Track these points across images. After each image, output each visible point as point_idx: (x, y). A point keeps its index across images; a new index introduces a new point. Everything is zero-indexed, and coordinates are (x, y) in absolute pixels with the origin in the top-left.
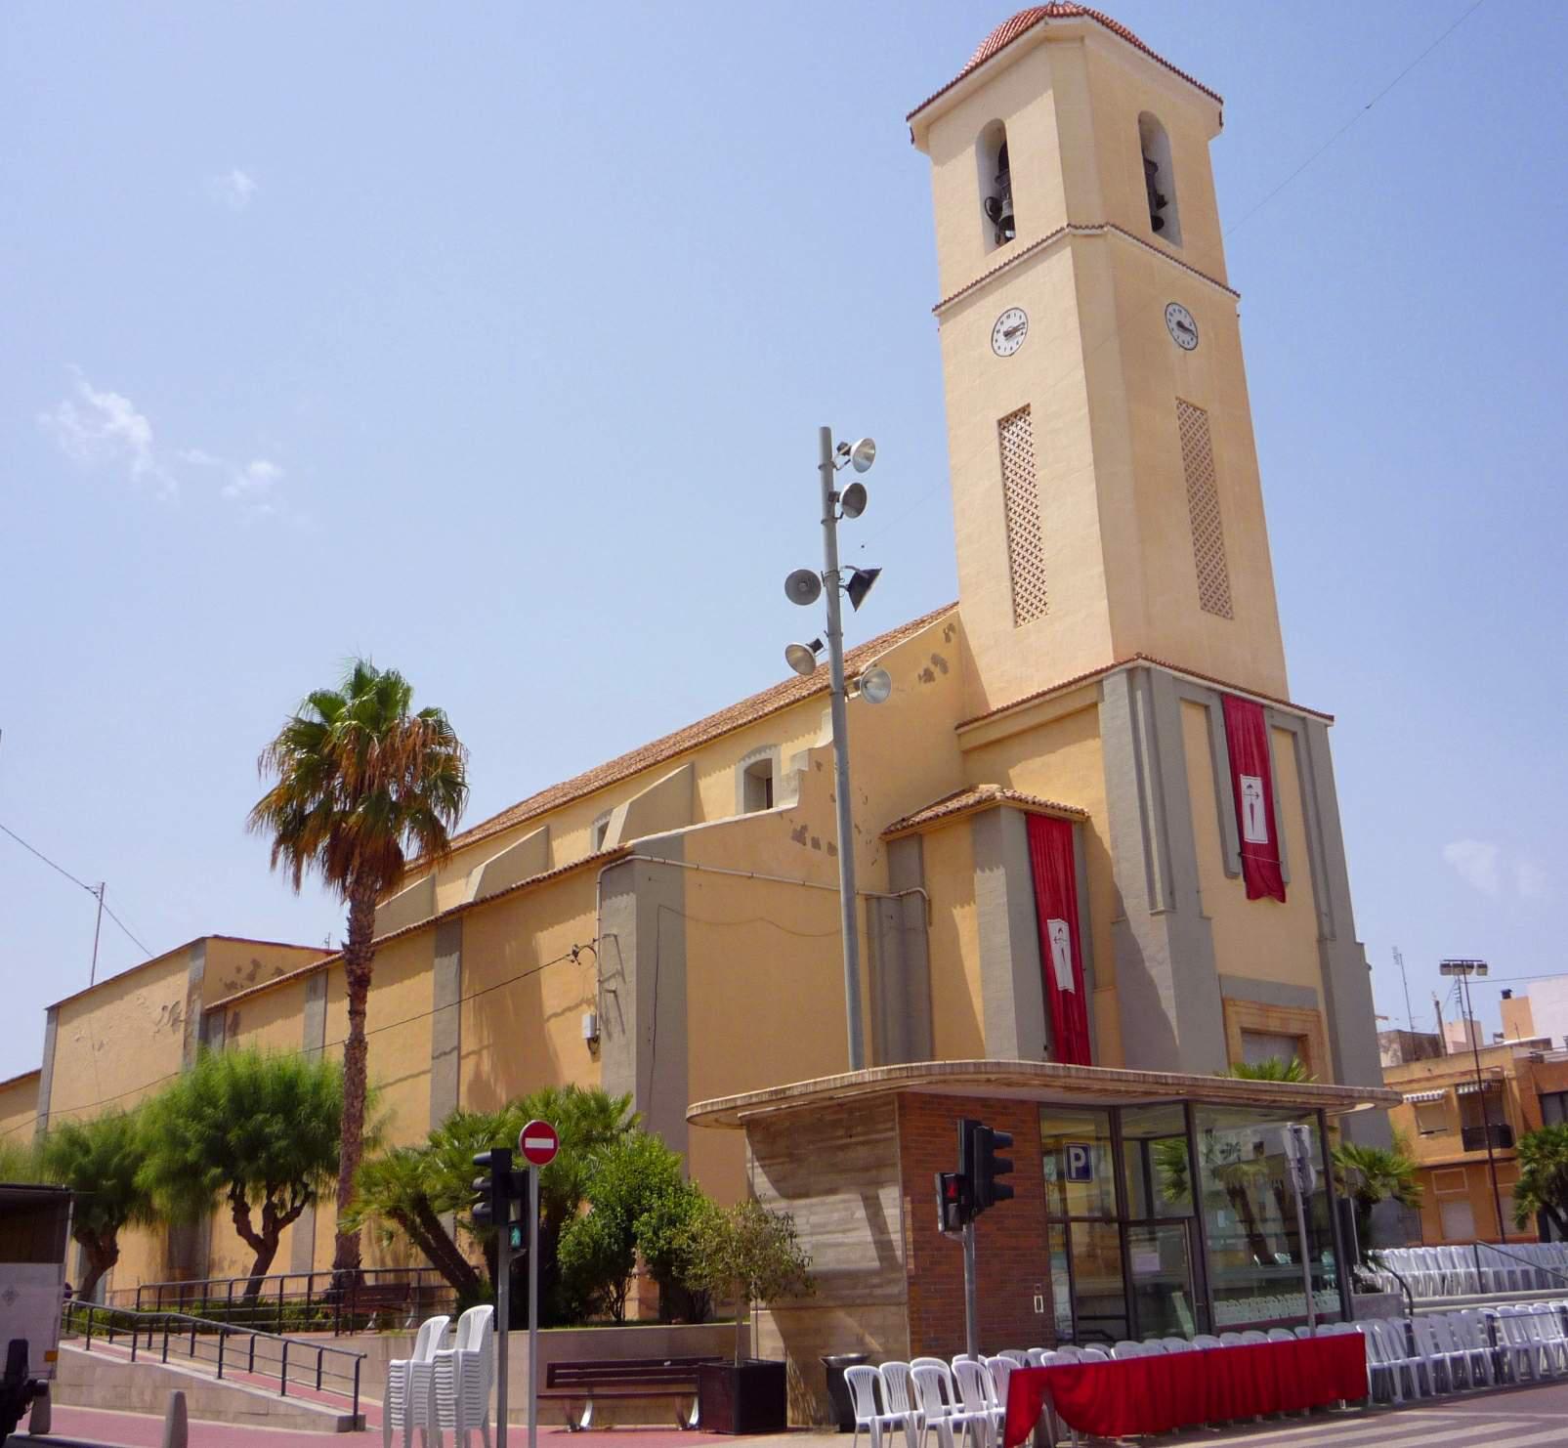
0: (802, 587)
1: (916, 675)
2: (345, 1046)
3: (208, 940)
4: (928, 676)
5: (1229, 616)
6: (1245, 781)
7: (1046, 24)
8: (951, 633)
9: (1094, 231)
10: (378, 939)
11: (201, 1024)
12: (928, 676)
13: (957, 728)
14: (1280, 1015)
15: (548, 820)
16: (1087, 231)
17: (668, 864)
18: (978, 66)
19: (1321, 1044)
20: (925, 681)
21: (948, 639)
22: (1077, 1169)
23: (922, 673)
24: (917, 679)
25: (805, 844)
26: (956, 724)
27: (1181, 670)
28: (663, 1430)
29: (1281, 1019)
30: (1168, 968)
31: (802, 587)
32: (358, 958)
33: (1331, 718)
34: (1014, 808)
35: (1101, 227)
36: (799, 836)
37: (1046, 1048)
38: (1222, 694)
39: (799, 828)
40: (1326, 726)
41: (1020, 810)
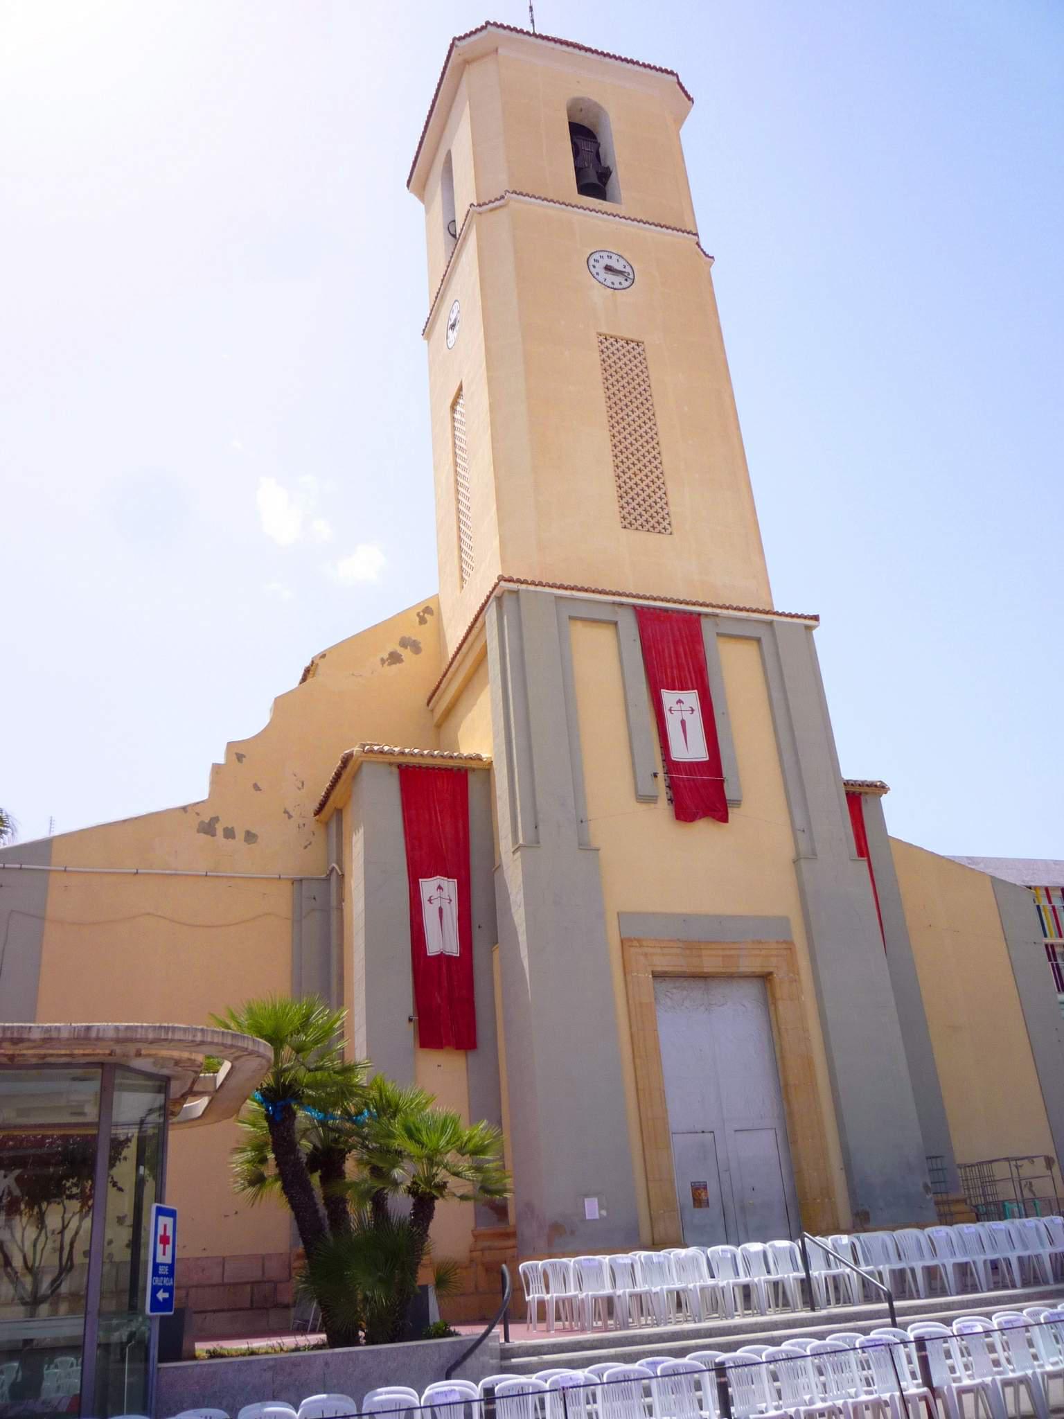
1: (378, 658)
4: (395, 658)
5: (668, 532)
9: (497, 203)
12: (395, 658)
14: (721, 953)
16: (491, 205)
17: (25, 869)
19: (795, 980)
20: (390, 664)
21: (422, 621)
23: (386, 656)
25: (213, 835)
26: (426, 701)
28: (976, 1270)
29: (723, 956)
30: (522, 910)
33: (816, 618)
34: (384, 762)
35: (502, 197)
36: (208, 828)
37: (410, 1020)
38: (634, 607)
40: (809, 629)
41: (391, 764)
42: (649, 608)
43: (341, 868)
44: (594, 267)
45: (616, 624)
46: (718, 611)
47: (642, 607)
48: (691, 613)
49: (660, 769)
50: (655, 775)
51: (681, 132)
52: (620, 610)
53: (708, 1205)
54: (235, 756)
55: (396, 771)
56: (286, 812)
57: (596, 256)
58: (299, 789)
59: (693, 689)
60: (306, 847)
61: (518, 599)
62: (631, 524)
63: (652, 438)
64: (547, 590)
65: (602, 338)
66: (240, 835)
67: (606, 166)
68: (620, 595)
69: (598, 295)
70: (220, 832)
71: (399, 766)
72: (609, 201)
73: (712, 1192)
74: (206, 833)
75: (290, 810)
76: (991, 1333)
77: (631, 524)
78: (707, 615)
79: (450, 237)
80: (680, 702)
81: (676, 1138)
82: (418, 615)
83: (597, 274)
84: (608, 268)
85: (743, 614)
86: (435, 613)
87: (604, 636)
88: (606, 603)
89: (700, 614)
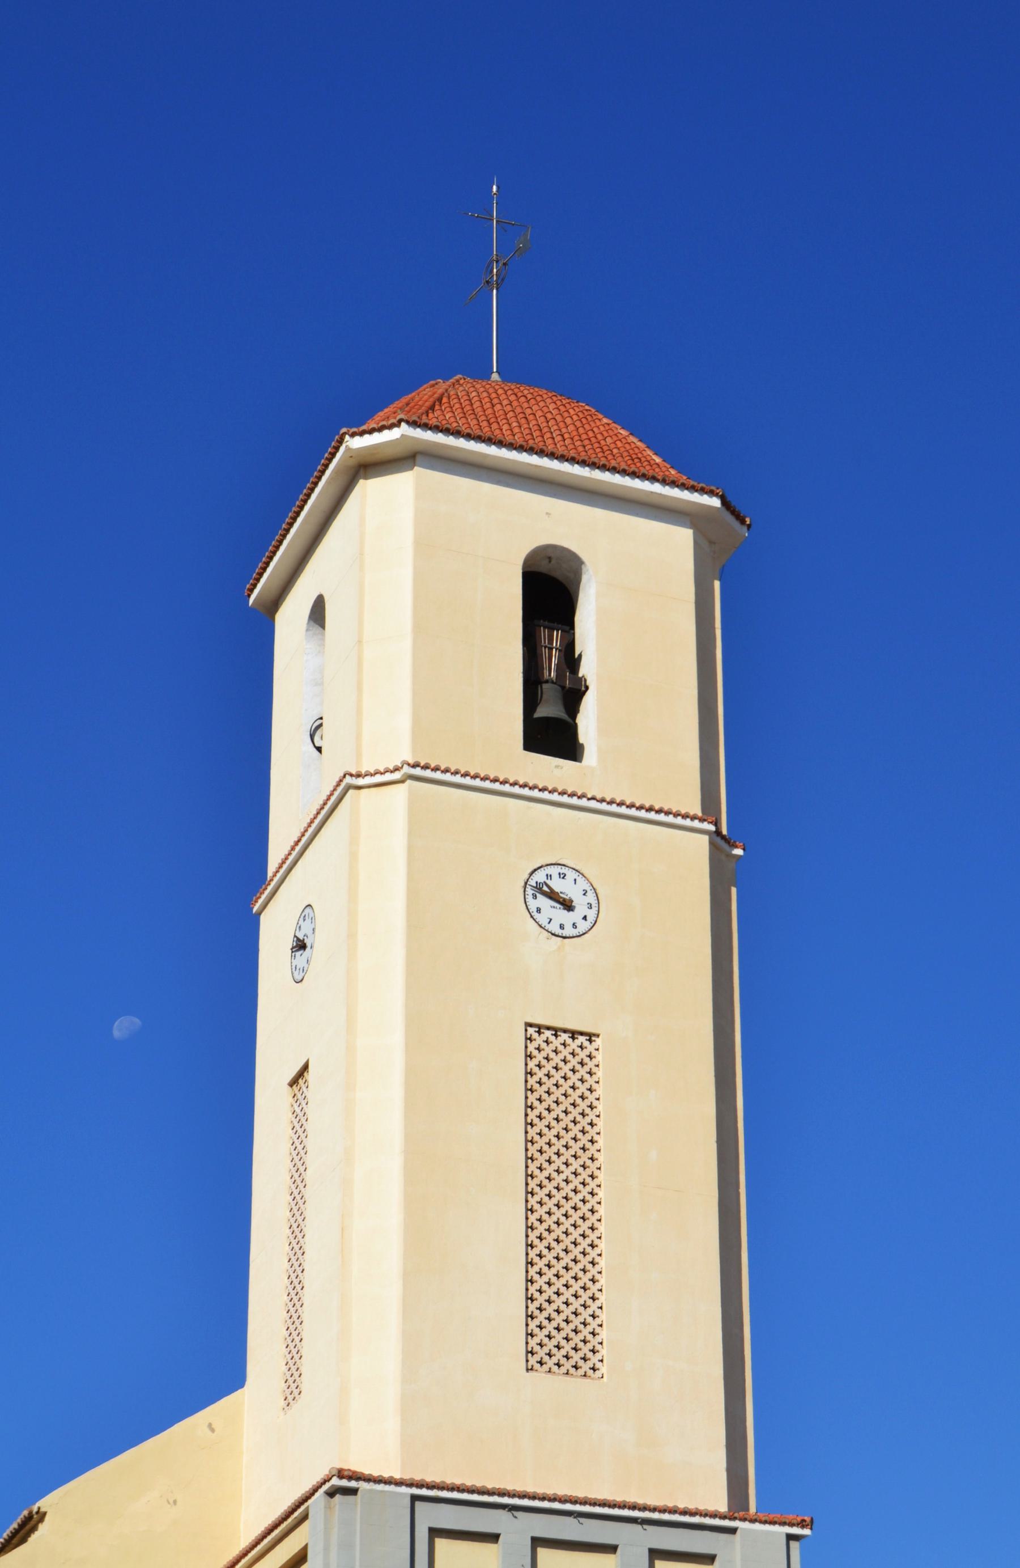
84: (568, 905)
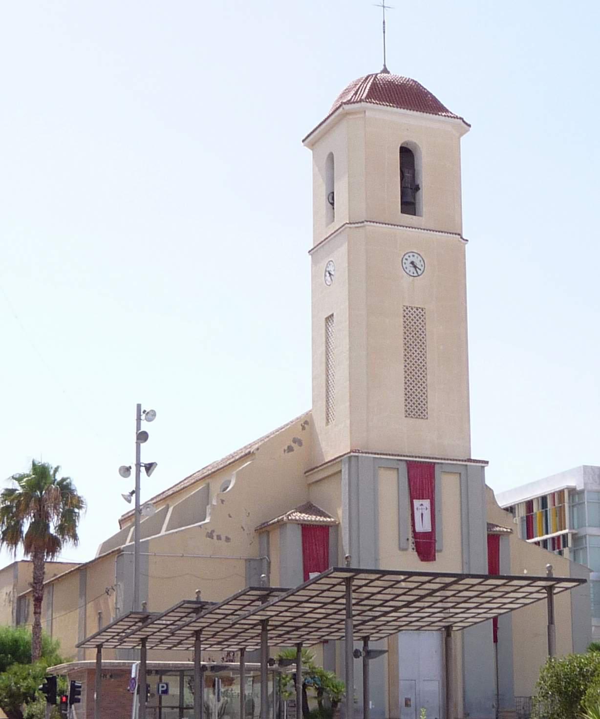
0: (125, 471)
2: (33, 626)
3: (19, 563)
4: (290, 449)
6: (417, 503)
7: (343, 108)
8: (305, 425)
10: (47, 582)
11: (17, 603)
12: (290, 449)
13: (305, 473)
15: (208, 481)
18: (332, 114)
20: (288, 452)
21: (304, 428)
22: (162, 691)
23: (286, 448)
24: (283, 452)
25: (212, 538)
26: (306, 470)
27: (378, 454)
31: (125, 471)
32: (36, 590)
35: (363, 222)
36: (210, 535)
38: (406, 461)
39: (209, 532)
40: (483, 467)
41: (298, 524)
42: (413, 461)
43: (269, 558)
44: (405, 263)
45: (398, 469)
46: (443, 461)
47: (410, 461)
48: (431, 463)
49: (410, 536)
50: (408, 539)
51: (462, 138)
52: (400, 462)
53: (410, 706)
54: (220, 501)
55: (300, 527)
56: (242, 528)
57: (407, 257)
58: (248, 516)
59: (428, 499)
60: (250, 544)
61: (358, 459)
62: (409, 414)
63: (424, 366)
64: (370, 455)
65: (405, 308)
66: (223, 538)
67: (417, 184)
68: (401, 456)
69: (406, 280)
70: (215, 537)
71: (302, 525)
72: (418, 216)
73: (412, 702)
74: (209, 537)
75: (244, 526)
76: (84, 597)
77: (409, 414)
78: (438, 463)
79: (329, 205)
80: (422, 505)
81: (401, 683)
82: (302, 425)
83: (406, 268)
84: (412, 263)
85: (455, 462)
86: (310, 423)
87: (393, 475)
88: (395, 460)
89: (435, 463)
